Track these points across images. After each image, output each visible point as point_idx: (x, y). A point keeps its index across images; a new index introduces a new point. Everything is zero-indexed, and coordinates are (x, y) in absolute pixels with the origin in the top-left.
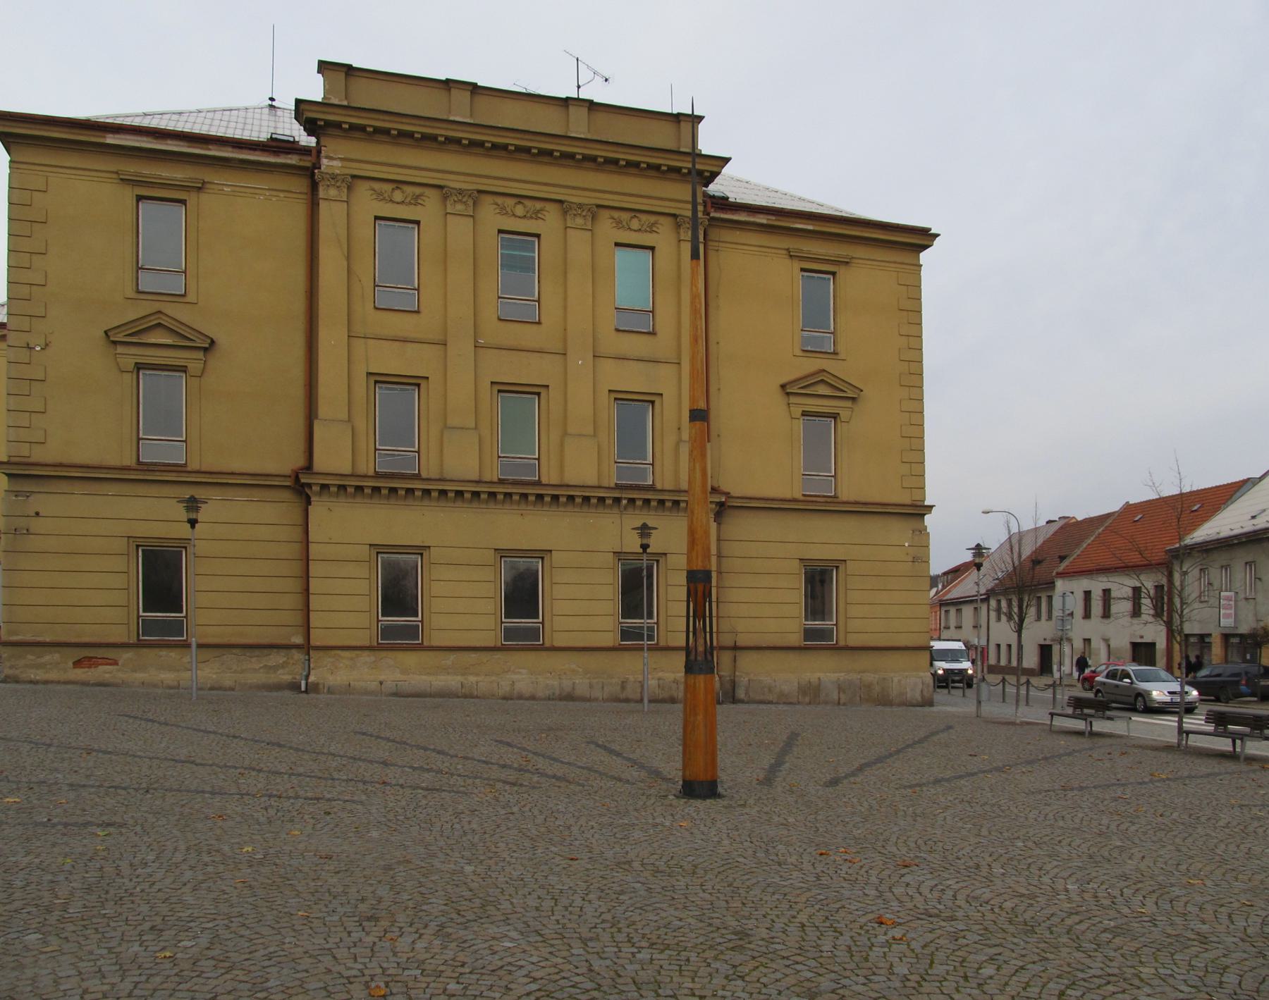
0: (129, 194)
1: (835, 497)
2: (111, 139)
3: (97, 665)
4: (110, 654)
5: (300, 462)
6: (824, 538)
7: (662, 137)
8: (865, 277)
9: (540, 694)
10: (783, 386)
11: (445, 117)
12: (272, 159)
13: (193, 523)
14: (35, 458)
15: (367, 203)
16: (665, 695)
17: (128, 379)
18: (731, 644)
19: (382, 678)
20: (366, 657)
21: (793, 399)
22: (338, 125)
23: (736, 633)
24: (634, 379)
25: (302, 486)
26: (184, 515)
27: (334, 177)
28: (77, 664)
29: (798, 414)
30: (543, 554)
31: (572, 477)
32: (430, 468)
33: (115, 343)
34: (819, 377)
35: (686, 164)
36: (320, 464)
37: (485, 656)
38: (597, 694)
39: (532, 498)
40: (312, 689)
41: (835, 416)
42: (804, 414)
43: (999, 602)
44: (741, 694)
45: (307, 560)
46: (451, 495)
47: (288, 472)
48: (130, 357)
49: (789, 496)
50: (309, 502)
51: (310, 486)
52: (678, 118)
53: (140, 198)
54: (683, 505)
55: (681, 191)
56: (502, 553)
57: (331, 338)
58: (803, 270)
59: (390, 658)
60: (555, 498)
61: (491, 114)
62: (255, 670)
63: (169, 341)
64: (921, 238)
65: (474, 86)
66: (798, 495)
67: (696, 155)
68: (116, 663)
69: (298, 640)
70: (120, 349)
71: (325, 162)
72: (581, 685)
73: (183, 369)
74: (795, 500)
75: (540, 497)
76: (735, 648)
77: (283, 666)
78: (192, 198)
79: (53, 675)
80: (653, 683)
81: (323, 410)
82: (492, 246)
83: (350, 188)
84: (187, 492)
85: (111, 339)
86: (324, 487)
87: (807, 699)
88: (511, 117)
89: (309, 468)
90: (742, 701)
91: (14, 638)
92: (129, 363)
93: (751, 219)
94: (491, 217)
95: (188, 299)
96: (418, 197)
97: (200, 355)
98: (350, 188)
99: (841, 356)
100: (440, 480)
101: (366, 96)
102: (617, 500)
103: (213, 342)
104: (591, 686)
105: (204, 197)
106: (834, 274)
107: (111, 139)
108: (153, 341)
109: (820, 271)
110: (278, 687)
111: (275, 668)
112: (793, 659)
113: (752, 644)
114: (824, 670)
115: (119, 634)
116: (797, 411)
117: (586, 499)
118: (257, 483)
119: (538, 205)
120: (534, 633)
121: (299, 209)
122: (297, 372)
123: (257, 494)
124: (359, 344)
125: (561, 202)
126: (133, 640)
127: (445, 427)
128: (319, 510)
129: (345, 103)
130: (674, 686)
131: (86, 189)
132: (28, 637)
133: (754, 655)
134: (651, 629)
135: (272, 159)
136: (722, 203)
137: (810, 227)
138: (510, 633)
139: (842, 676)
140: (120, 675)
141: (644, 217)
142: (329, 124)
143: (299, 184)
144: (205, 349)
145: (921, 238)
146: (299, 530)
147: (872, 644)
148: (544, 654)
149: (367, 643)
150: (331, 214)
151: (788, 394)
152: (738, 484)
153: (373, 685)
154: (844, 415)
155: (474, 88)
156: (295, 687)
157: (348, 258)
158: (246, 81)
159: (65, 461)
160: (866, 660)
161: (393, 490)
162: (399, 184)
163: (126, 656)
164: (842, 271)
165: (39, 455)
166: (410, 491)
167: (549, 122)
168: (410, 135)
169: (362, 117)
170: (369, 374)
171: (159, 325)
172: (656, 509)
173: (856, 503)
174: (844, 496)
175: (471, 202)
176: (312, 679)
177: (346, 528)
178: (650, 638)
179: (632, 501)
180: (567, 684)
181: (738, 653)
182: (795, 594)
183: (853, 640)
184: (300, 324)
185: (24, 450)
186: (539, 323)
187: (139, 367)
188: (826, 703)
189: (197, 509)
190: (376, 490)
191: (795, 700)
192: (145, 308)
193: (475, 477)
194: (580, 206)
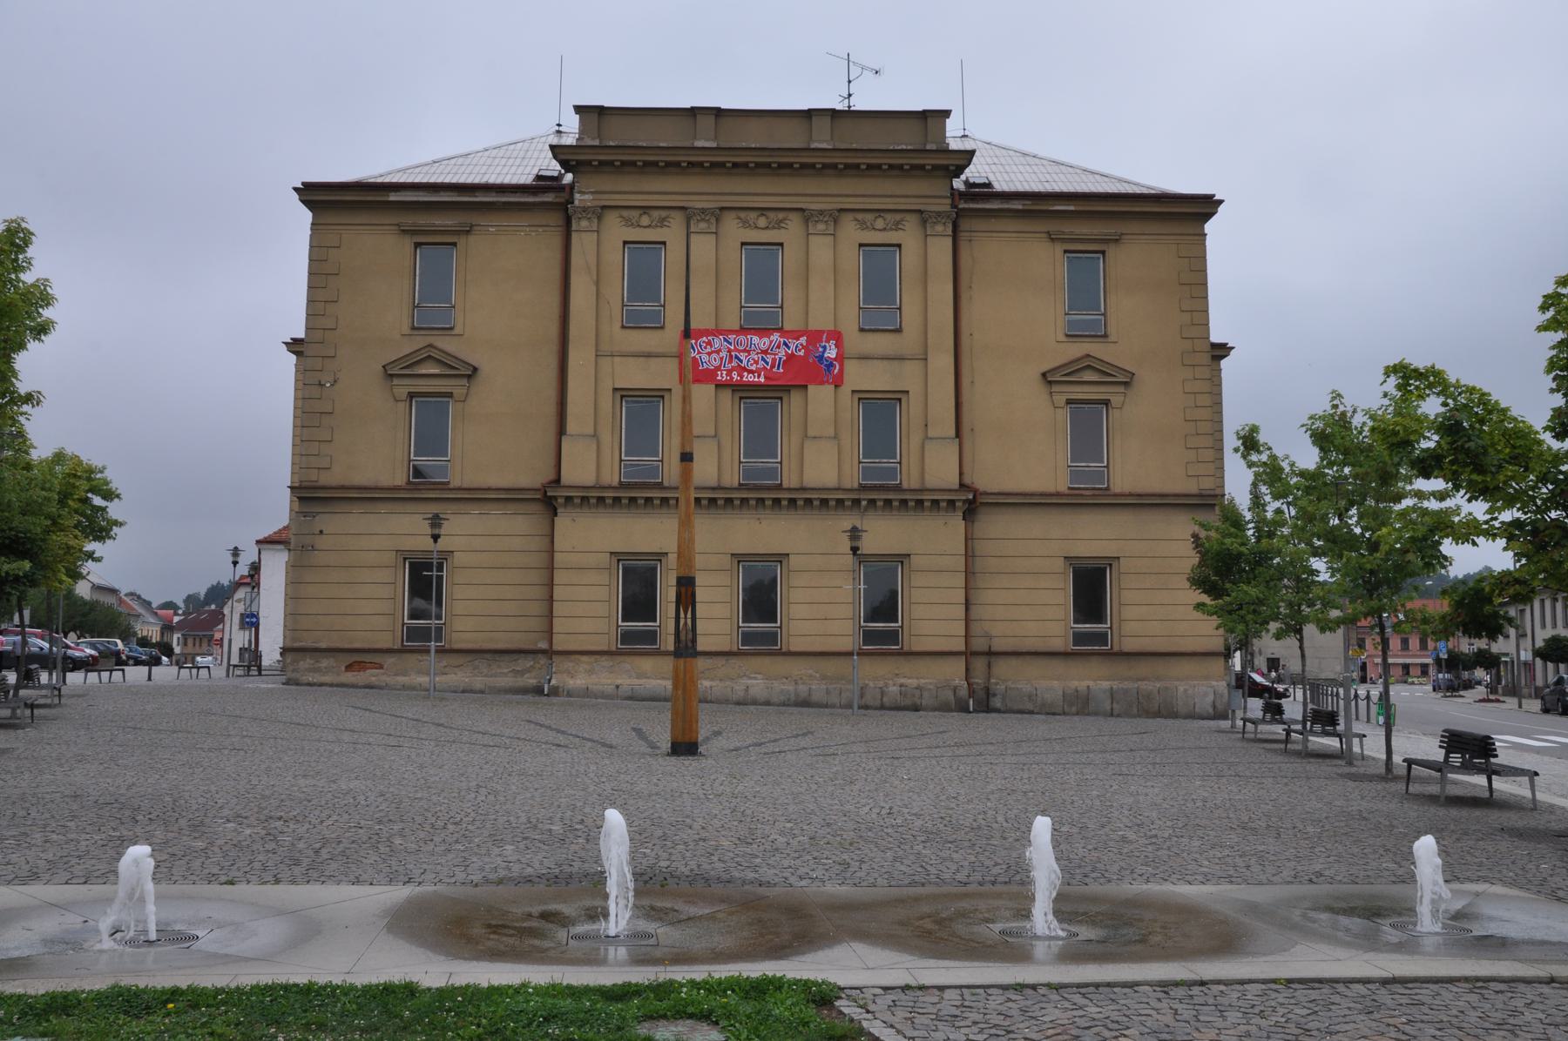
0: (408, 243)
1: (1107, 489)
2: (393, 197)
3: (365, 669)
4: (377, 659)
5: (552, 476)
6: (1093, 536)
7: (905, 139)
8: (1136, 258)
9: (775, 700)
10: (1044, 375)
11: (687, 144)
12: (531, 199)
13: (436, 538)
14: (321, 483)
15: (616, 231)
16: (908, 702)
17: (403, 406)
18: (986, 649)
19: (619, 682)
20: (605, 662)
21: (1055, 388)
22: (589, 163)
23: (991, 637)
24: (636, 376)
25: (550, 499)
26: (429, 531)
27: (585, 209)
28: (349, 668)
29: (1063, 403)
30: (781, 558)
31: (931, 482)
32: (910, 480)
33: (392, 376)
34: (1087, 363)
35: (929, 161)
36: (567, 477)
37: (720, 661)
38: (835, 700)
39: (768, 503)
40: (555, 692)
41: (1107, 403)
42: (1069, 402)
43: (1542, 601)
44: (997, 702)
45: (551, 568)
46: (593, 501)
47: (538, 485)
48: (403, 388)
49: (1052, 489)
50: (556, 514)
51: (555, 498)
52: (924, 115)
53: (417, 245)
54: (672, 502)
55: (935, 187)
56: (739, 558)
57: (580, 359)
58: (1066, 252)
59: (628, 663)
60: (793, 501)
61: (643, 136)
62: (505, 675)
63: (436, 371)
64: (1205, 206)
65: (602, 108)
66: (1063, 488)
67: (947, 151)
68: (381, 667)
69: (543, 645)
70: (396, 381)
71: (577, 196)
72: (818, 690)
73: (450, 395)
74: (1058, 494)
75: (777, 501)
76: (990, 653)
77: (528, 671)
78: (461, 241)
79: (327, 679)
80: (893, 689)
81: (572, 426)
82: (852, 261)
83: (600, 218)
84: (434, 508)
85: (388, 375)
86: (569, 499)
87: (1074, 709)
88: (753, 137)
89: (558, 481)
90: (998, 711)
91: (296, 645)
92: (402, 392)
93: (1006, 206)
94: (852, 234)
95: (456, 331)
96: (664, 219)
97: (464, 382)
98: (836, 221)
99: (1112, 338)
100: (838, 489)
101: (618, 135)
102: (856, 502)
103: (475, 369)
104: (828, 692)
105: (472, 238)
106: (1103, 252)
107: (393, 197)
108: (424, 371)
109: (422, 240)
110: (524, 691)
111: (522, 673)
112: (1058, 666)
113: (1009, 649)
114: (1092, 678)
115: (385, 641)
116: (1061, 399)
117: (824, 502)
118: (509, 497)
119: (781, 215)
120: (771, 638)
121: (556, 241)
122: (551, 393)
123: (511, 508)
124: (605, 363)
125: (802, 210)
126: (397, 646)
127: (927, 438)
128: (563, 522)
129: (597, 143)
130: (918, 693)
131: (380, 247)
132: (309, 644)
133: (1014, 662)
134: (439, 630)
135: (531, 199)
136: (982, 192)
137: (1072, 208)
138: (748, 638)
139: (1115, 685)
140: (384, 678)
141: (889, 216)
142: (579, 163)
143: (555, 219)
144: (469, 377)
145: (1205, 206)
146: (547, 540)
147: (1162, 650)
148: (780, 659)
149: (605, 648)
150: (583, 244)
151: (1050, 383)
152: (985, 480)
153: (610, 689)
154: (1116, 400)
155: (718, 112)
156: (538, 691)
157: (597, 283)
158: (509, 136)
159: (347, 483)
160: (1143, 668)
161: (633, 500)
162: (645, 209)
163: (390, 661)
164: (1112, 251)
165: (325, 479)
166: (648, 500)
167: (790, 137)
168: (611, 163)
169: (619, 154)
170: (615, 390)
171: (1089, 367)
172: (899, 509)
173: (1130, 495)
174: (1117, 487)
175: (713, 220)
176: (553, 682)
177: (590, 539)
178: (439, 639)
179: (872, 502)
180: (803, 689)
181: (993, 659)
182: (1060, 597)
183: (1129, 645)
184: (554, 347)
185: (313, 475)
186: (1106, 336)
187: (411, 396)
188: (1096, 714)
189: (439, 526)
190: (744, 501)
191: (1059, 710)
192: (419, 342)
193: (713, 483)
194: (821, 212)
